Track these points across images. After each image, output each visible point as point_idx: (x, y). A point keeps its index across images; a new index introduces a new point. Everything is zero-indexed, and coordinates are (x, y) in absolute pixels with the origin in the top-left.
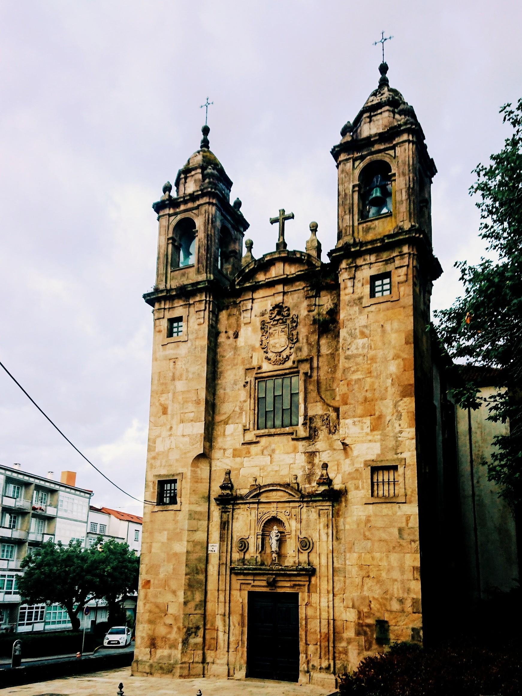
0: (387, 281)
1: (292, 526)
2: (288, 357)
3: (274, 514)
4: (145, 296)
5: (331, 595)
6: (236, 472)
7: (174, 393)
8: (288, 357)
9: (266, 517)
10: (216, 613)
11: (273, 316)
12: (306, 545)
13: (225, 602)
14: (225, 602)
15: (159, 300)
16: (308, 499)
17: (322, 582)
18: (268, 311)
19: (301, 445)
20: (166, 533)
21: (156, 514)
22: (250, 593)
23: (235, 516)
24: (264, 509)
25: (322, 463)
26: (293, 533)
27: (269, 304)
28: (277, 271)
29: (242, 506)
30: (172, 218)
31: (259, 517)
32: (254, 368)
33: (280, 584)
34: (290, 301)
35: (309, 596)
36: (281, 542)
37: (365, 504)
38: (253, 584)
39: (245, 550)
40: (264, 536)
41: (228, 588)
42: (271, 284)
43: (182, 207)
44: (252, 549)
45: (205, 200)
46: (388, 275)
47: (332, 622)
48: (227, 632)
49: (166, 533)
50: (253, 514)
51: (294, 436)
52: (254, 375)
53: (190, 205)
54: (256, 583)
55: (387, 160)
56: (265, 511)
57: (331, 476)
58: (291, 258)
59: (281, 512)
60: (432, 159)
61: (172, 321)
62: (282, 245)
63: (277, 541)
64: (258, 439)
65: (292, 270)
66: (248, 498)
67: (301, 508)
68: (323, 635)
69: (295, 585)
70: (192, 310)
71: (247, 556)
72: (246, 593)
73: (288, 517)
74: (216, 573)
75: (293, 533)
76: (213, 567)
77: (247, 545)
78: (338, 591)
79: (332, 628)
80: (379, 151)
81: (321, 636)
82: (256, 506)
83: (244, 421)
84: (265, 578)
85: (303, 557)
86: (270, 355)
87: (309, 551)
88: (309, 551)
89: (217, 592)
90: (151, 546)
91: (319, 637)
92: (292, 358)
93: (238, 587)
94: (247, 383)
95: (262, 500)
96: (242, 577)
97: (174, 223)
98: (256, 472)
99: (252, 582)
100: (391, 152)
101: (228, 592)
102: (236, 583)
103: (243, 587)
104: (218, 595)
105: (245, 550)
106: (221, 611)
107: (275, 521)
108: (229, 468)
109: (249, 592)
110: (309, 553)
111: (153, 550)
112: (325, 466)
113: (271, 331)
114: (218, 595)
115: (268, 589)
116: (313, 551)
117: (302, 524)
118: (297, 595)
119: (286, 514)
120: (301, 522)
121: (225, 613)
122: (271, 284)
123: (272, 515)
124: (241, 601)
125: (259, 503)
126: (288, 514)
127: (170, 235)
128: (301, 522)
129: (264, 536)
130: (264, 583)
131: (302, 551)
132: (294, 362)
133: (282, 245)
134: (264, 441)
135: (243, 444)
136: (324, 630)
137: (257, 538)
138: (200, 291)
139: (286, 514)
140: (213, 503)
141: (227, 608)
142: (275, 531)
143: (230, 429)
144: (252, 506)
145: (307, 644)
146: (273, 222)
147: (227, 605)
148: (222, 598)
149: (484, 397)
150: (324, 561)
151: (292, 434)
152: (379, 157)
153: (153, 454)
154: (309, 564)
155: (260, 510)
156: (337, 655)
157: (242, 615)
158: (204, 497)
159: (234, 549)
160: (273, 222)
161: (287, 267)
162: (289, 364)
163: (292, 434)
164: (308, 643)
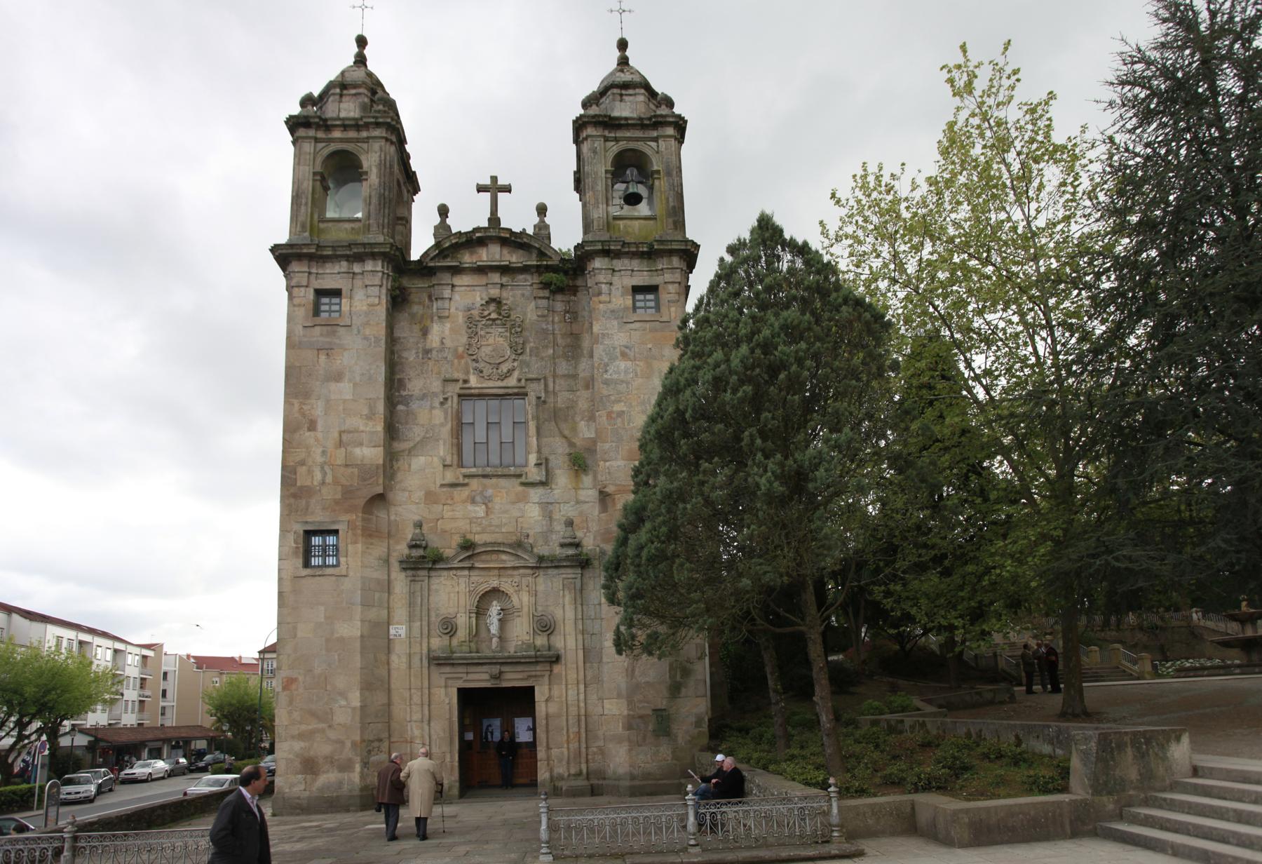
0: (650, 297)
1: (522, 600)
2: (510, 372)
4: (275, 249)
5: (582, 687)
7: (328, 401)
8: (510, 372)
11: (486, 313)
12: (546, 626)
15: (300, 257)
16: (543, 564)
17: (570, 670)
18: (478, 305)
19: (535, 494)
20: (322, 608)
21: (304, 581)
23: (433, 587)
26: (525, 609)
27: (478, 297)
28: (488, 255)
29: (445, 573)
30: (320, 145)
32: (457, 381)
34: (508, 296)
40: (480, 611)
42: (481, 270)
43: (337, 134)
44: (462, 634)
45: (377, 132)
46: (653, 289)
49: (322, 608)
50: (463, 586)
51: (523, 479)
52: (457, 390)
53: (352, 134)
54: (471, 677)
55: (649, 152)
57: (579, 534)
58: (513, 240)
61: (320, 293)
62: (494, 220)
64: (466, 481)
65: (514, 258)
68: (572, 756)
70: (358, 282)
71: (455, 642)
72: (455, 691)
74: (404, 666)
75: (525, 609)
76: (399, 657)
80: (637, 139)
82: (466, 572)
83: (442, 453)
84: (485, 668)
85: (541, 641)
86: (481, 365)
90: (295, 628)
92: (516, 374)
94: (446, 399)
95: (477, 565)
96: (448, 669)
97: (326, 152)
98: (463, 525)
100: (653, 144)
102: (439, 676)
103: (450, 682)
106: (417, 716)
107: (495, 592)
109: (460, 690)
111: (299, 634)
112: (570, 523)
113: (482, 333)
118: (532, 689)
122: (481, 270)
127: (318, 169)
129: (480, 611)
132: (519, 380)
133: (494, 220)
134: (475, 483)
135: (442, 486)
138: (373, 256)
140: (395, 566)
141: (426, 712)
142: (495, 609)
143: (419, 462)
144: (459, 573)
145: (548, 748)
146: (481, 189)
147: (426, 708)
148: (416, 699)
149: (833, 202)
150: (571, 643)
151: (520, 476)
152: (632, 145)
153: (292, 490)
154: (549, 648)
155: (473, 579)
158: (380, 559)
159: (432, 632)
160: (481, 189)
161: (505, 251)
162: (512, 381)
163: (520, 476)
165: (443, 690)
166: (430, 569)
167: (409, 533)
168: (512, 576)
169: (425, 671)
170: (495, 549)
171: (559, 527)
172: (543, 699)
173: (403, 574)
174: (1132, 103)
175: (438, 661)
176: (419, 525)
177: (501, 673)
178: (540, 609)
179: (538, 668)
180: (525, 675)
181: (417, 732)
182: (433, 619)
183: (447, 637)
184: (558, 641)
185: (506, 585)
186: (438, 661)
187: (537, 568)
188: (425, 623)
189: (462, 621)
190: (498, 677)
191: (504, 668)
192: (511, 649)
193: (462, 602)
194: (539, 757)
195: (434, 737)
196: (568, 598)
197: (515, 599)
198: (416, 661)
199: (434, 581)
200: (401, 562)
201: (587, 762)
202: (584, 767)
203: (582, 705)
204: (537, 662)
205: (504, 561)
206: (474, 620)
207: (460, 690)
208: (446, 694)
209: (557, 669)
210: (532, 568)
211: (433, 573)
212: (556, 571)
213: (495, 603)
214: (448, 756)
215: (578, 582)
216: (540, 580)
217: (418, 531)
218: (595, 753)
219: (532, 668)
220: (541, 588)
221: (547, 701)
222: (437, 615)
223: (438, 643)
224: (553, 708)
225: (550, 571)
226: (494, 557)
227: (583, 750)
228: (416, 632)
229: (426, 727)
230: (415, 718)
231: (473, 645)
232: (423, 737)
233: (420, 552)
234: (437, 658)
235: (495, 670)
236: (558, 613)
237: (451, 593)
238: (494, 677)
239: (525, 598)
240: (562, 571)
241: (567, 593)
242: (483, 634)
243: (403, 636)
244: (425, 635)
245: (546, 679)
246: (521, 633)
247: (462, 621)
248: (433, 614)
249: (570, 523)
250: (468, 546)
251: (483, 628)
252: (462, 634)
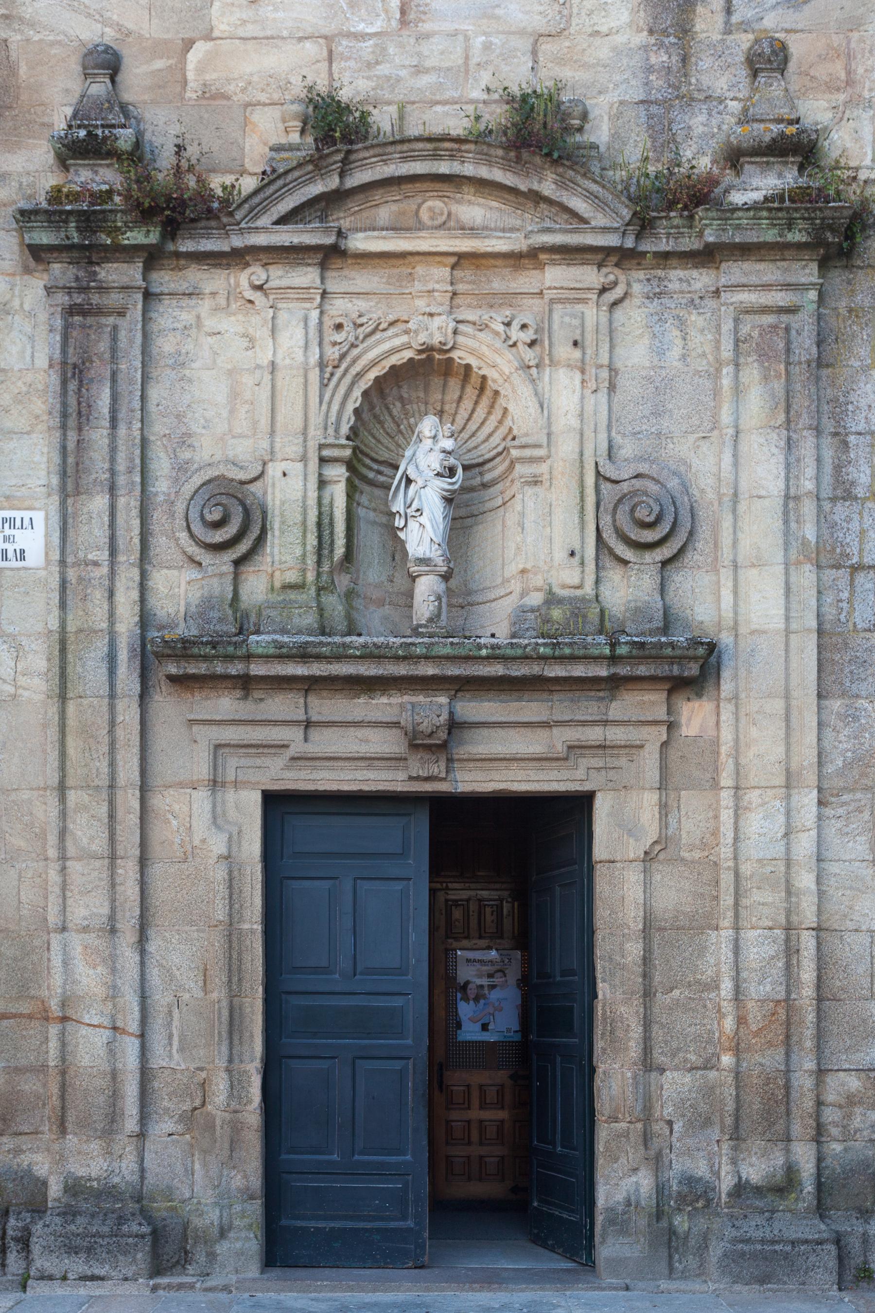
3: (436, 330)
6: (159, 64)
9: (389, 349)
10: (53, 918)
12: (650, 523)
13: (113, 857)
14: (113, 857)
22: (274, 802)
23: (165, 345)
24: (361, 304)
25: (745, 40)
29: (215, 281)
31: (333, 353)
33: (386, 743)
35: (664, 808)
36: (468, 505)
37: (596, 463)
38: (298, 747)
39: (243, 547)
40: (366, 463)
41: (129, 770)
44: (286, 554)
47: (808, 942)
48: (134, 1026)
54: (325, 742)
56: (375, 311)
59: (483, 327)
60: (232, 249)
63: (448, 500)
66: (265, 221)
67: (615, 304)
68: (754, 1104)
69: (575, 749)
71: (256, 587)
73: (529, 355)
77: (257, 516)
78: (840, 773)
79: (808, 974)
81: (741, 1020)
82: (307, 276)
84: (385, 706)
85: (627, 591)
87: (665, 552)
88: (665, 552)
89: (53, 800)
91: (729, 1024)
93: (202, 770)
95: (359, 242)
96: (226, 704)
99: (295, 734)
101: (130, 800)
102: (189, 731)
103: (232, 764)
104: (63, 814)
105: (243, 547)
106: (88, 907)
107: (428, 374)
108: (109, 36)
110: (665, 563)
114: (63, 814)
115: (402, 776)
116: (691, 557)
117: (618, 398)
118: (582, 803)
119: (515, 333)
120: (612, 388)
121: (112, 918)
123: (422, 338)
124: (218, 845)
125: (331, 255)
126: (528, 336)
128: (612, 388)
129: (366, 463)
130: (386, 743)
131: (621, 550)
136: (763, 988)
137: (322, 483)
139: (515, 333)
141: (130, 891)
142: (426, 454)
144: (280, 276)
145: (648, 1064)
147: (129, 871)
148: (88, 832)
155: (339, 307)
156: (830, 1115)
157: (231, 932)
159: (161, 544)
164: (659, 1058)
165: (201, 798)
166: (152, 258)
167: (59, 98)
168: (510, 298)
169: (128, 713)
170: (434, 167)
171: (721, 76)
172: (635, 849)
173: (37, 284)
174: (469, 593)
175: (183, 662)
176: (107, 63)
177: (454, 725)
178: (627, 449)
179: (617, 709)
180: (561, 737)
181: (90, 978)
182: (161, 486)
183: (224, 562)
184: (705, 599)
185: (484, 351)
186: (183, 662)
187: (623, 257)
188: (128, 503)
189: (290, 492)
190: (441, 743)
191: (472, 709)
192: (496, 623)
193: (290, 413)
194: (603, 1105)
195: (161, 999)
196: (756, 400)
197: (521, 408)
198: (90, 670)
199: (171, 316)
200: (26, 216)
201: (819, 1134)
202: (804, 1157)
203: (806, 880)
204: (615, 684)
205: (472, 231)
206: (338, 493)
207: (263, 791)
208: (216, 820)
209: (695, 716)
210: (602, 256)
211: (165, 280)
212: (702, 279)
213: (428, 425)
214: (220, 1086)
215: (804, 325)
216: (634, 316)
217: (99, 88)
218: (851, 1101)
219: (589, 708)
220: (635, 354)
221: (648, 857)
222: (182, 469)
223: (181, 589)
224: (672, 893)
225: (677, 277)
226: (433, 205)
227: (803, 1082)
228: (92, 534)
229: (129, 958)
230: (79, 913)
231: (334, 604)
232: (113, 994)
233: (104, 177)
234: (183, 649)
235: (433, 709)
236: (705, 467)
237: (243, 370)
238: (421, 743)
239: (565, 391)
240: (735, 271)
241: (752, 373)
242: (373, 572)
243: (36, 556)
244: (129, 556)
245: (650, 759)
246: (540, 549)
247: (290, 492)
248: (162, 465)
249: (769, 60)
250: (334, 127)
251: (370, 540)
252: (286, 554)
